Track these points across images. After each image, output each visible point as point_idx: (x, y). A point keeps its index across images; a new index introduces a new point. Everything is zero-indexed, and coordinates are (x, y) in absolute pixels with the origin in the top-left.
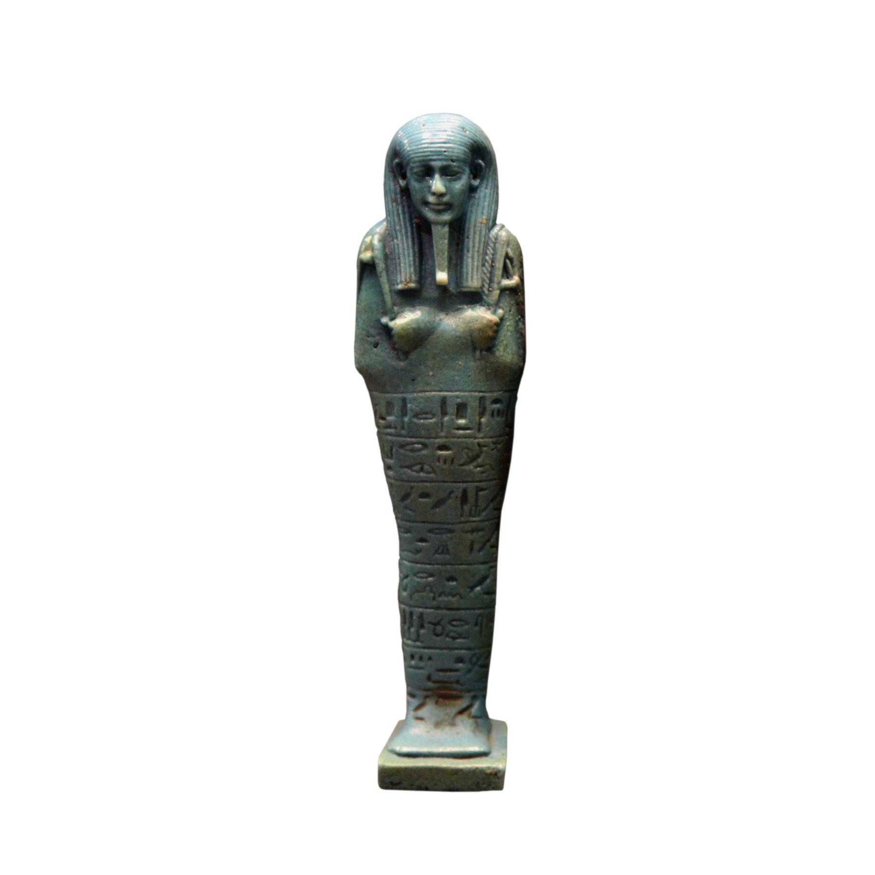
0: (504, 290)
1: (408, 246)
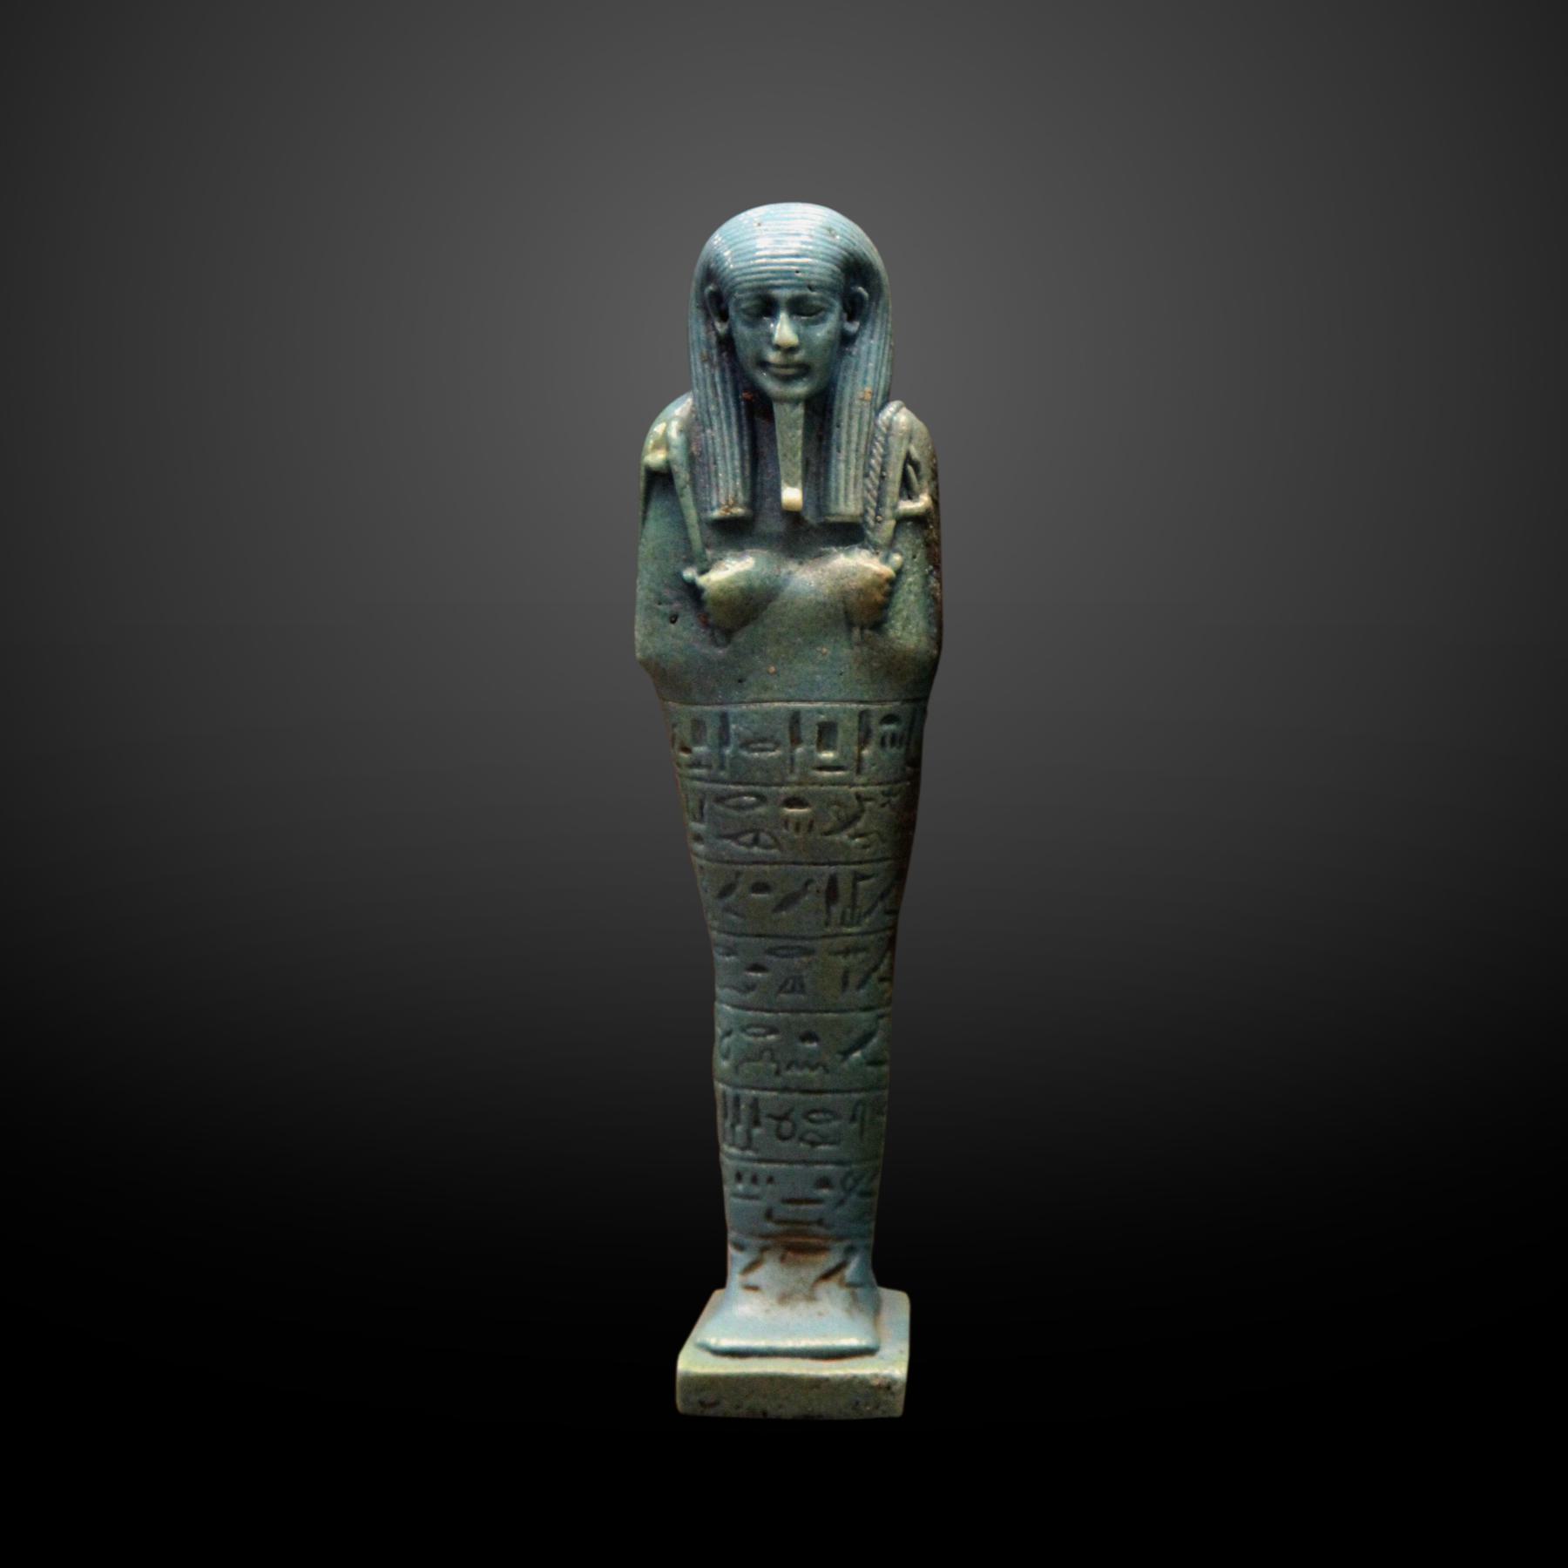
0: (903, 520)
1: (731, 441)
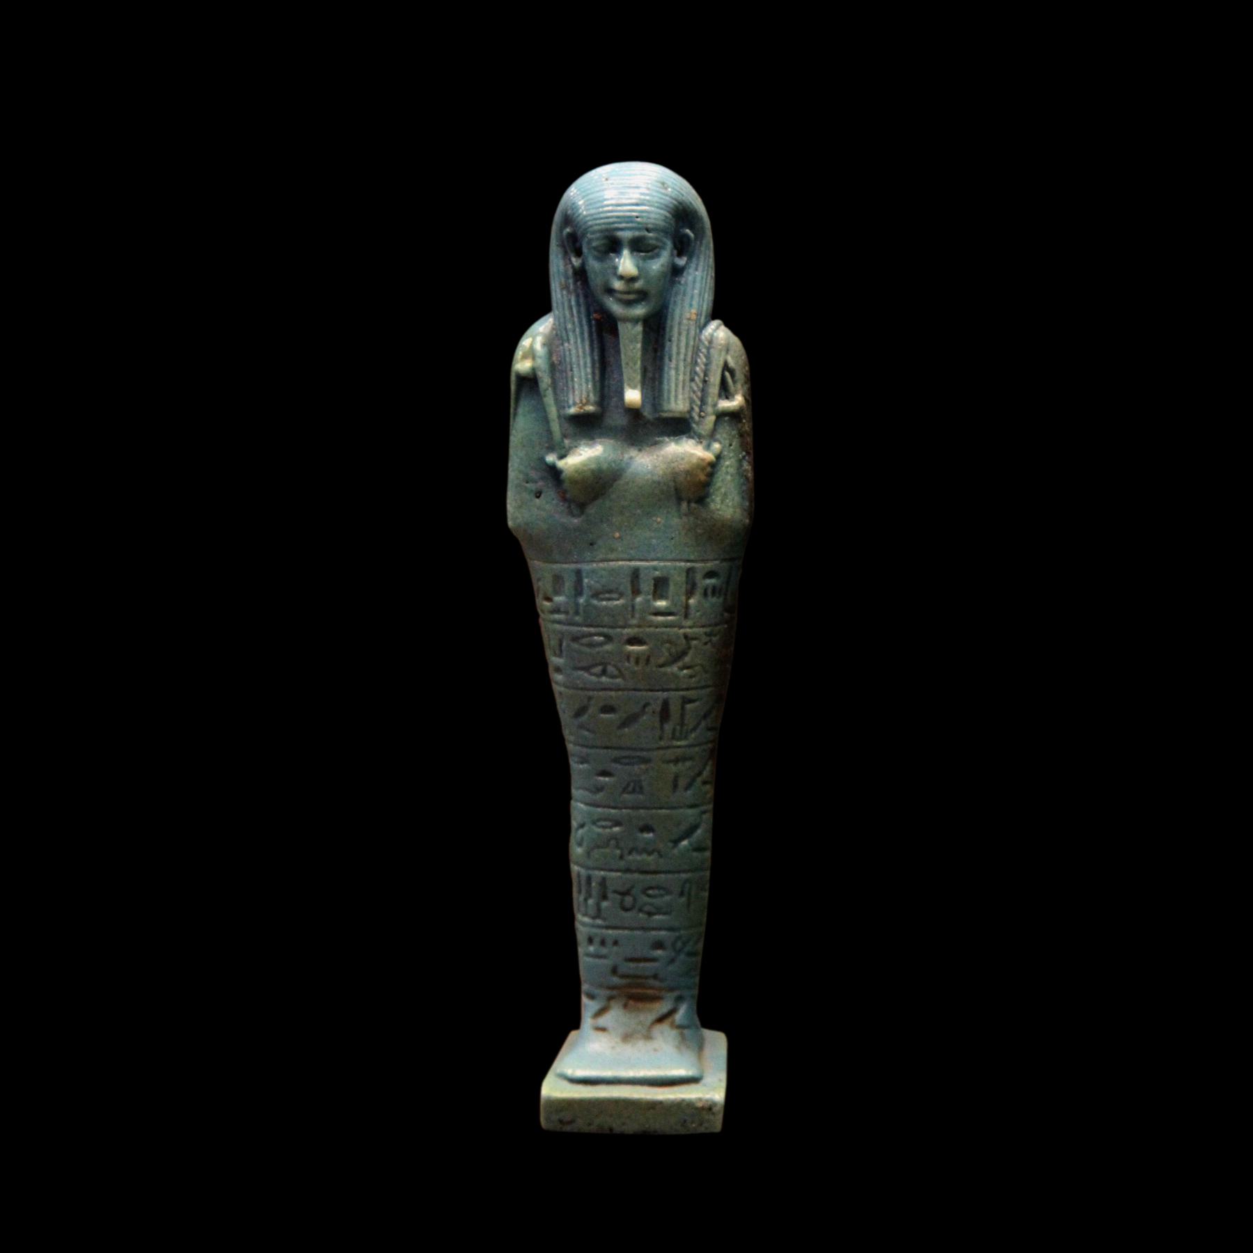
0: (721, 416)
1: (584, 353)
